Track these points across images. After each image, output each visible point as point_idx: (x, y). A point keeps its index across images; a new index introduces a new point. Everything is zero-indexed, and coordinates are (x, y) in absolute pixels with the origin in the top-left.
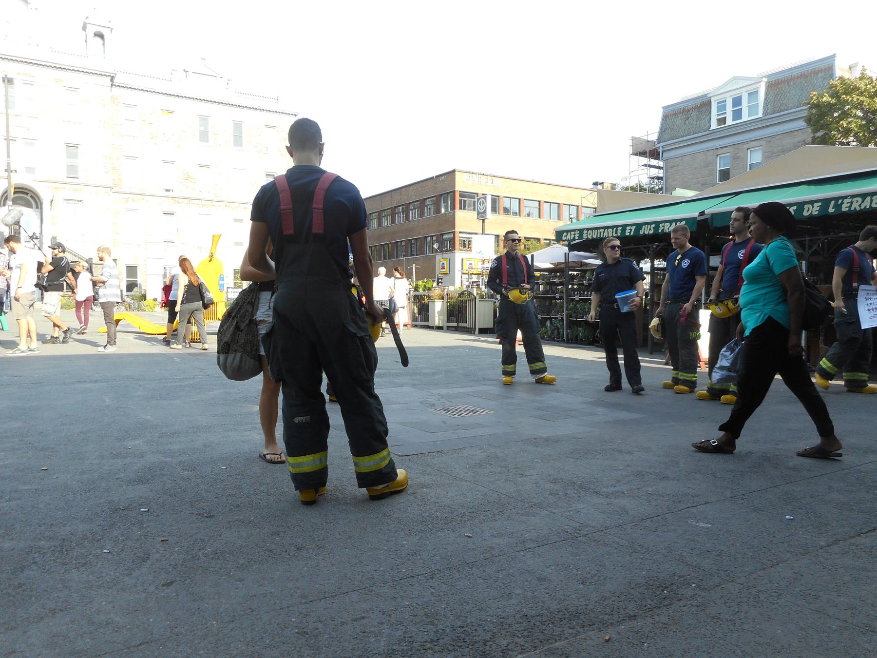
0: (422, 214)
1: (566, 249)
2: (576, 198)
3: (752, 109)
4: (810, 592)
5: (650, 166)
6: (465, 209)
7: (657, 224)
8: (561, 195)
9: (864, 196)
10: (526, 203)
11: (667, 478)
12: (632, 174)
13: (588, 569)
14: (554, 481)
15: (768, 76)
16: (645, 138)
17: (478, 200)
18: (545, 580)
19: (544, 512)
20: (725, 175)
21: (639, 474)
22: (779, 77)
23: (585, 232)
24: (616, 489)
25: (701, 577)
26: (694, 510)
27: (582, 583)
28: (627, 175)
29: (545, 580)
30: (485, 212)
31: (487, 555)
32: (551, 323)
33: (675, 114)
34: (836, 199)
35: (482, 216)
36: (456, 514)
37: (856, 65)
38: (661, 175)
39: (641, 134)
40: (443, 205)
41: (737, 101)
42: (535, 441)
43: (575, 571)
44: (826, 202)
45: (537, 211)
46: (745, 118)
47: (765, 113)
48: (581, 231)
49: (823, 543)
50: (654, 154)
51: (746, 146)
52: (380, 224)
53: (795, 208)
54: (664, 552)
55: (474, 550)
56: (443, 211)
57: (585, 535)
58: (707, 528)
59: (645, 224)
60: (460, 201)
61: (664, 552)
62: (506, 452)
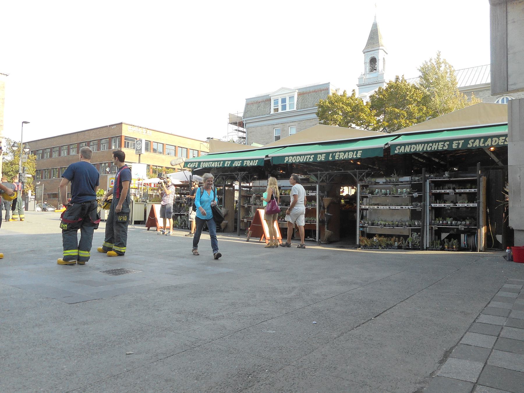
0: (99, 149)
1: (191, 174)
2: (196, 146)
3: (291, 105)
4: (331, 365)
5: (239, 131)
6: (128, 147)
7: (243, 160)
8: (188, 144)
9: (345, 152)
10: (167, 147)
11: (249, 305)
12: (229, 134)
13: (200, 369)
14: (180, 313)
15: (299, 89)
16: (237, 115)
17: (137, 142)
18: (170, 380)
19: (173, 333)
20: (278, 138)
21: (233, 304)
22: (304, 91)
23: (202, 163)
24: (219, 314)
25: (271, 365)
26: (265, 323)
27: (197, 379)
28: (227, 135)
29: (170, 380)
30: (141, 149)
31: (129, 368)
32: (181, 218)
33: (252, 104)
34: (333, 153)
35: (139, 153)
36: (108, 341)
37: (339, 89)
38: (245, 136)
39: (234, 112)
40: (113, 144)
41: (284, 101)
42: (168, 288)
43: (191, 372)
44: (328, 154)
45: (174, 151)
46: (288, 110)
47: (297, 108)
48: (200, 163)
49: (336, 336)
50: (241, 124)
51: (288, 125)
52: (68, 153)
53: (313, 156)
54: (249, 351)
55: (120, 365)
56: (113, 148)
57: (199, 346)
58: (274, 333)
59: (236, 160)
60: (125, 142)
61: (249, 351)
62: (148, 296)
